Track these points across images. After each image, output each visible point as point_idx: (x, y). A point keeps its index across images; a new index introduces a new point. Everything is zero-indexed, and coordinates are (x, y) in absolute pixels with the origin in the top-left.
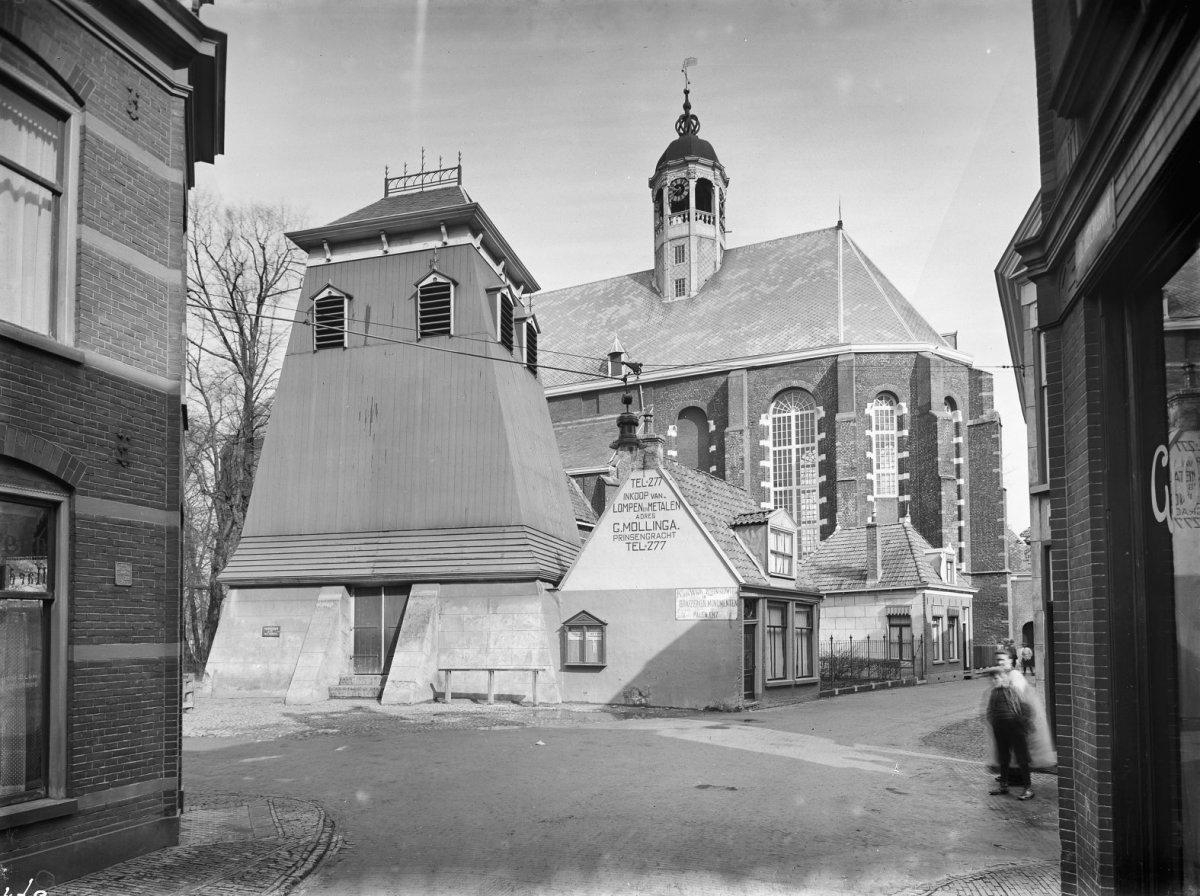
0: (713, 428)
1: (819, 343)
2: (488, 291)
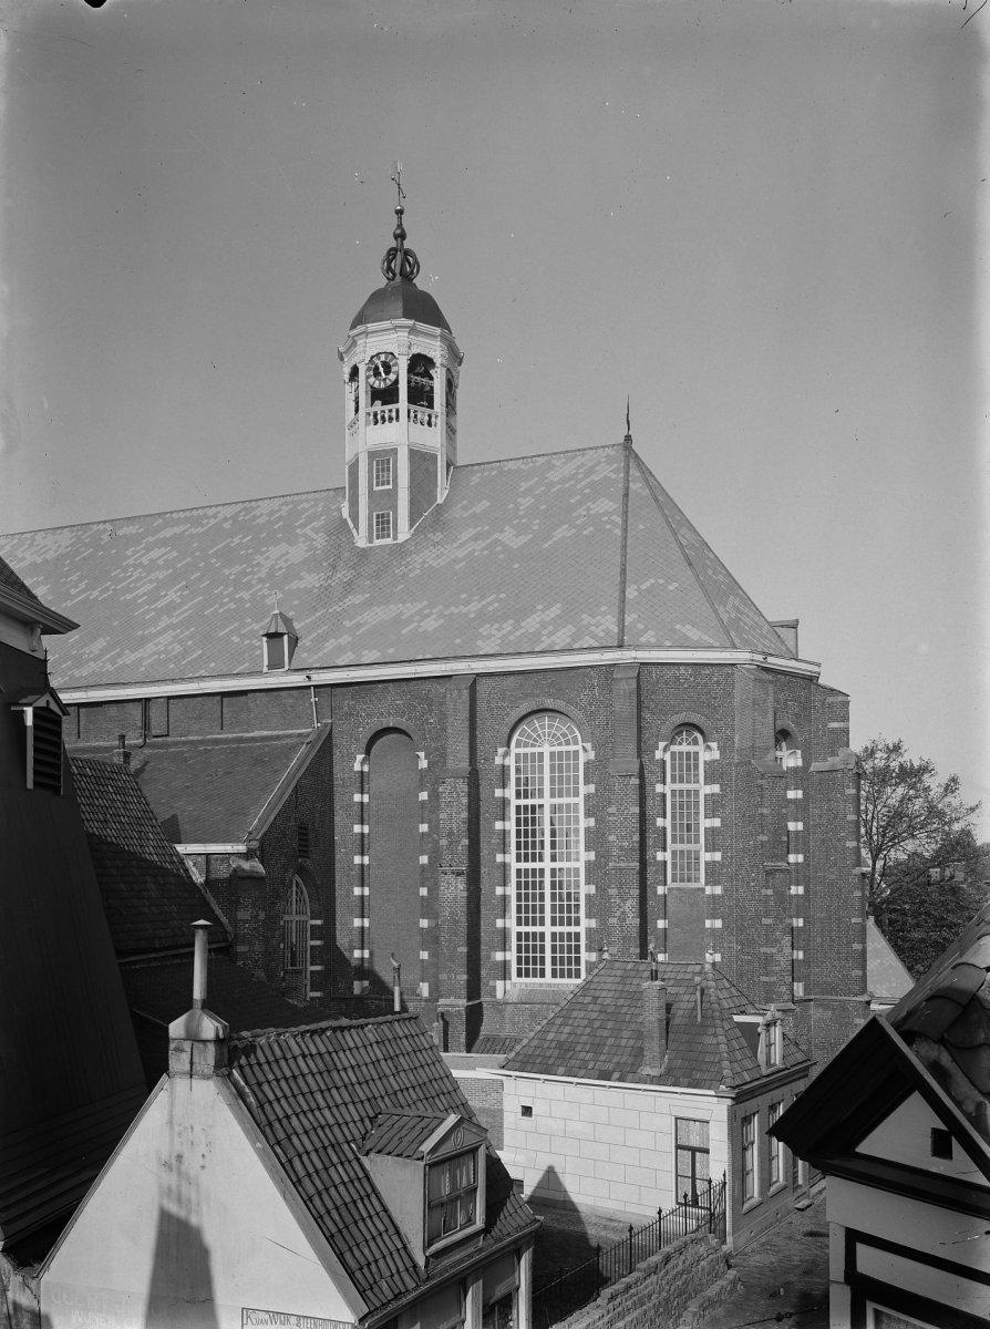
0: (423, 764)
1: (589, 642)
2: (269, 636)
